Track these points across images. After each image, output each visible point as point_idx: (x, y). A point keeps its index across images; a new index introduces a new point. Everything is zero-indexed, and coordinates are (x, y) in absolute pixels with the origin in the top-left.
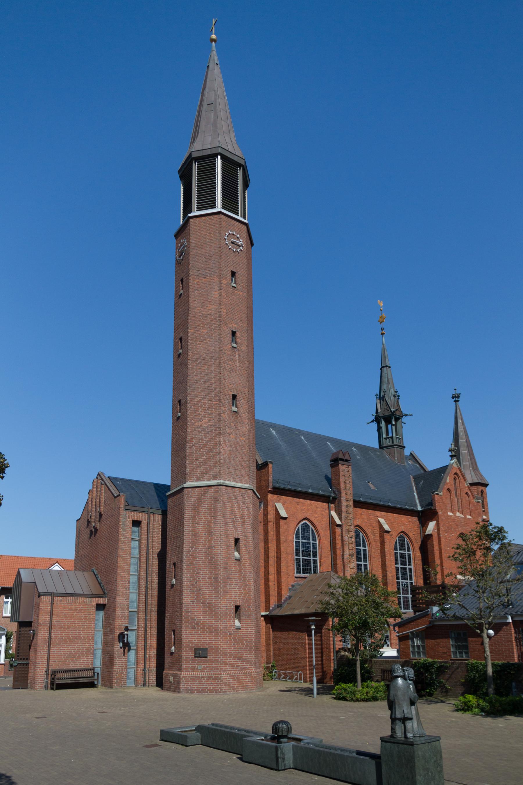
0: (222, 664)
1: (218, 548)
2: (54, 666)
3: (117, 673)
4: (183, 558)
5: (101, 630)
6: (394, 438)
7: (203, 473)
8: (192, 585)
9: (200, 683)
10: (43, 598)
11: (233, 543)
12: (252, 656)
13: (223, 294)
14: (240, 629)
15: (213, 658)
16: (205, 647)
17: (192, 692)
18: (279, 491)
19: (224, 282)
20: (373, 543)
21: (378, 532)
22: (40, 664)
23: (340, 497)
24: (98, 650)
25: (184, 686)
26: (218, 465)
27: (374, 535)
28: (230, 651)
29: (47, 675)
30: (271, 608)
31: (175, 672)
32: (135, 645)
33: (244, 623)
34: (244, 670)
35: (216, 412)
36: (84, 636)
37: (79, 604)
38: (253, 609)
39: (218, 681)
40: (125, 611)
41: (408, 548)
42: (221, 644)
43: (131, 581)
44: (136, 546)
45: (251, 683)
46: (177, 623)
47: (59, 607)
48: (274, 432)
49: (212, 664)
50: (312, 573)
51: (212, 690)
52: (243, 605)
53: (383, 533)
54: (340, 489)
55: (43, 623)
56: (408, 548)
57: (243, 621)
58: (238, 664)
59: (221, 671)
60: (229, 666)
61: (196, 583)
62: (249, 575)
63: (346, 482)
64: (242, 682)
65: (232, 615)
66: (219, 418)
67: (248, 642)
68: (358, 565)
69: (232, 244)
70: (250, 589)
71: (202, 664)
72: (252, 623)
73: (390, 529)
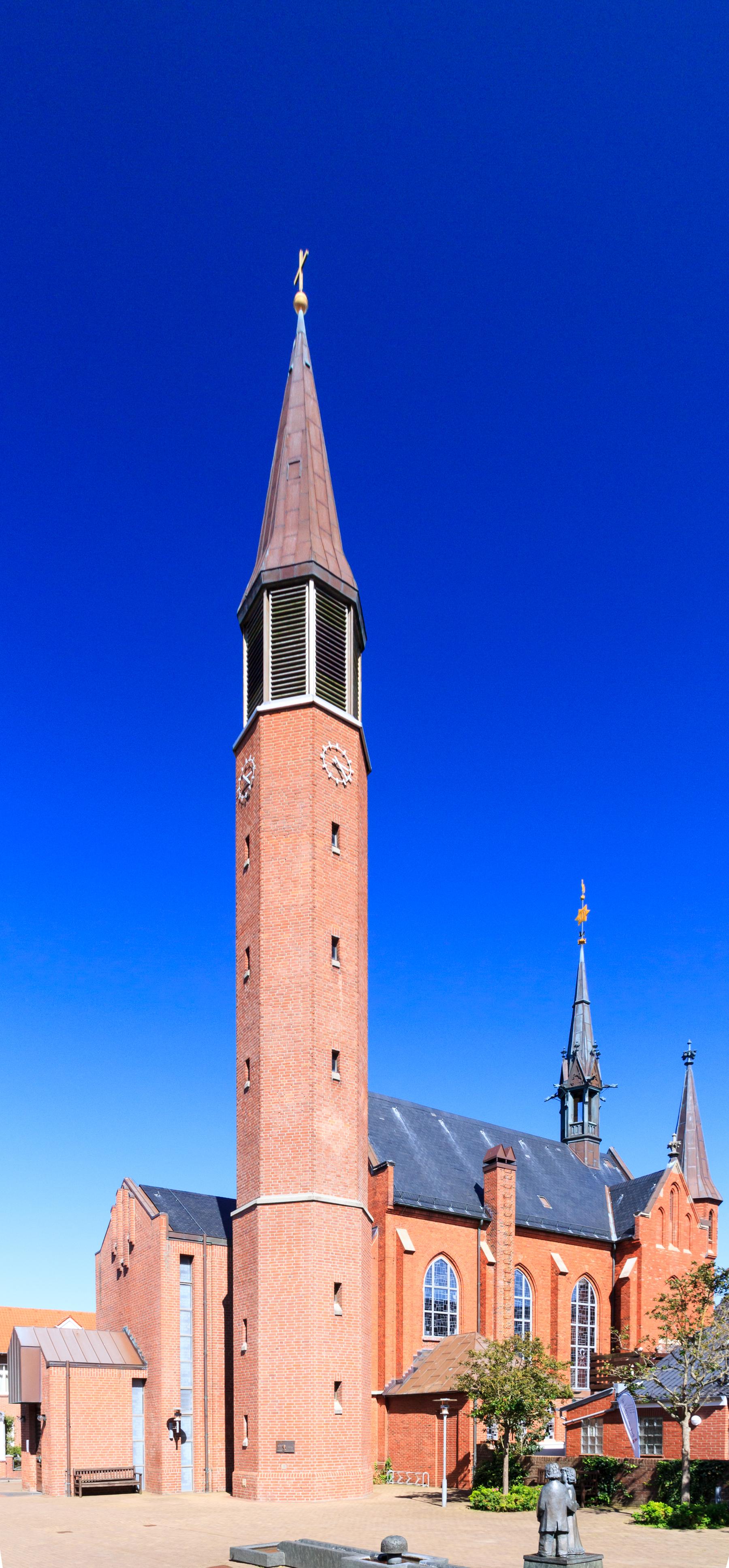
0: (315, 1462)
2: (76, 1466)
3: (167, 1474)
8: (272, 1352)
10: (54, 1370)
16: (292, 1439)
33: (347, 1407)
38: (360, 1387)
40: (175, 1388)
46: (250, 1406)
53: (557, 1275)
56: (592, 1298)
57: (346, 1404)
58: (338, 1462)
59: (313, 1472)
60: (325, 1465)
66: (310, 1091)
68: (516, 1323)
71: (288, 1463)
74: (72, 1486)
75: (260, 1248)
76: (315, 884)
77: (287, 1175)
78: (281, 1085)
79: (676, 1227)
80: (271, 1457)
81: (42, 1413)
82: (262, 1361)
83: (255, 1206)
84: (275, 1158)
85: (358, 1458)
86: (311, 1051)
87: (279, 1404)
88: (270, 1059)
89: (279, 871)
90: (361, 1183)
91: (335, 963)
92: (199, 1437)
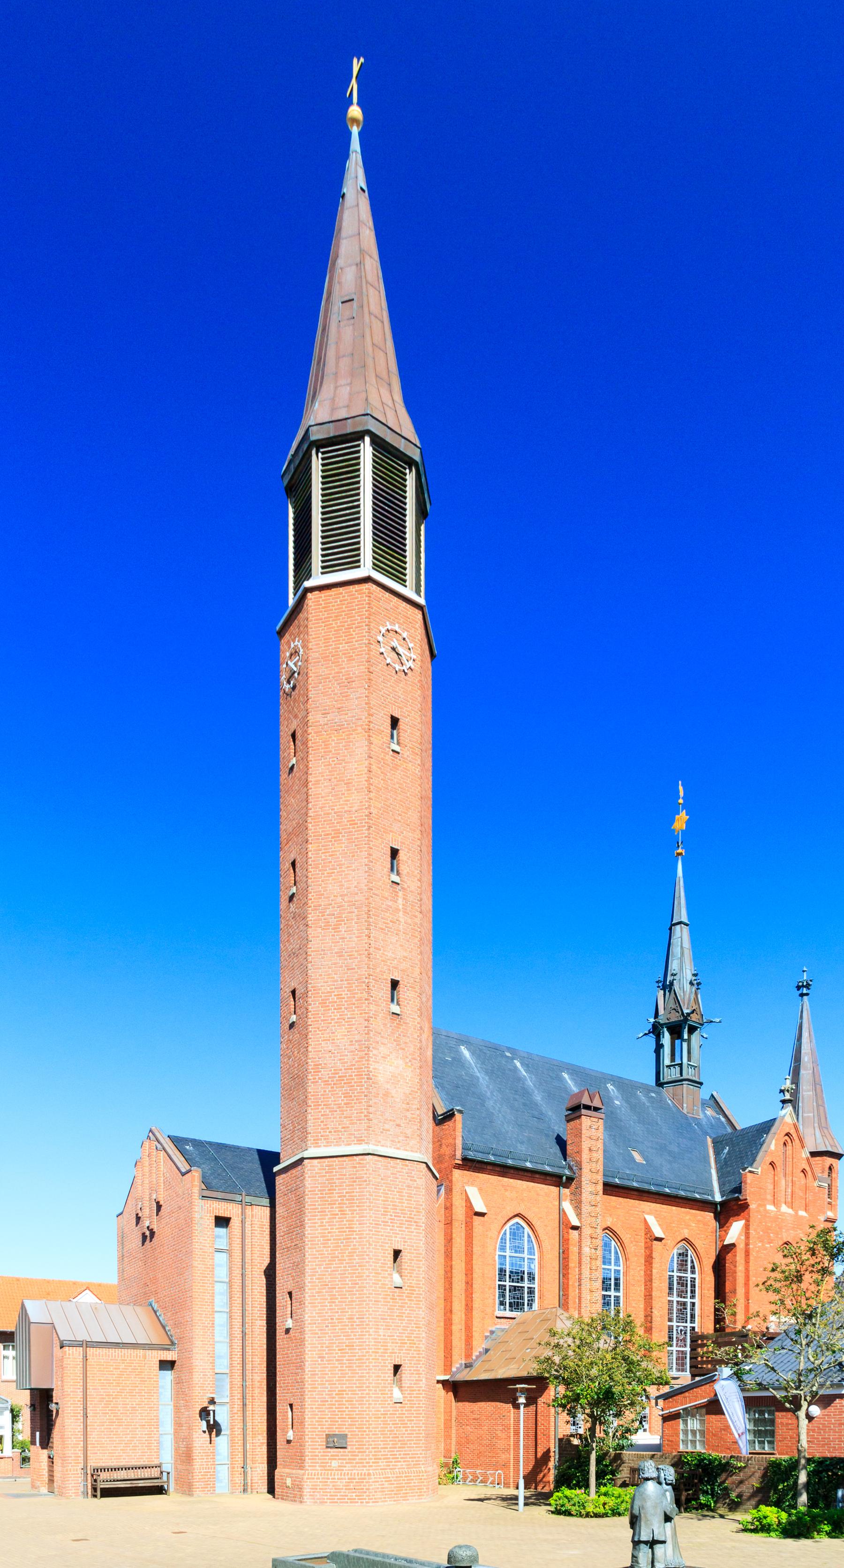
7: (338, 1131)
10: (69, 1350)
13: (374, 767)
30: (454, 1369)
38: (423, 1371)
43: (216, 1322)
53: (651, 1240)
56: (693, 1267)
59: (369, 1470)
62: (417, 1314)
64: (404, 1487)
66: (365, 1027)
68: (604, 1297)
71: (339, 1459)
75: (307, 1209)
76: (371, 787)
77: (339, 1124)
79: (790, 1184)
80: (320, 1452)
83: (302, 1160)
85: (421, 1454)
90: (424, 1133)
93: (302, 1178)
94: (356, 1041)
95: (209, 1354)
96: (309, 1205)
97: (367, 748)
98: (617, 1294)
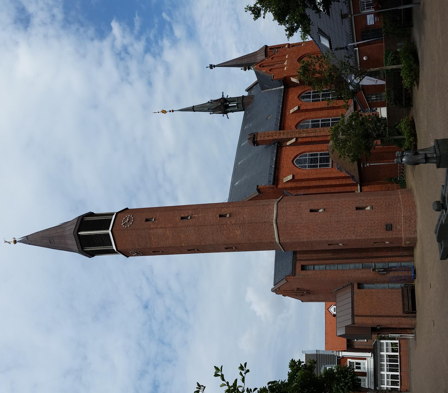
0: (397, 216)
1: (317, 221)
2: (400, 312)
3: (405, 274)
4: (325, 240)
5: (375, 285)
6: (238, 102)
9: (410, 227)
10: (356, 321)
11: (313, 213)
12: (390, 197)
13: (160, 226)
14: (372, 207)
15: (392, 221)
17: (416, 231)
18: (276, 179)
19: (152, 226)
20: (307, 116)
21: (299, 113)
22: (399, 322)
23: (277, 139)
24: (389, 286)
25: (412, 235)
26: (264, 223)
27: (301, 116)
28: (387, 212)
29: (406, 317)
30: (355, 182)
31: (403, 241)
32: (385, 263)
33: (368, 204)
34: (400, 202)
35: (231, 226)
36: (380, 296)
37: (358, 300)
38: (358, 198)
39: (408, 218)
40: (362, 271)
41: (308, 93)
42: (383, 217)
43: (341, 269)
44: (318, 267)
45: (409, 197)
46: (369, 241)
47: (361, 312)
48: (237, 183)
49: (397, 221)
50: (329, 156)
51: (414, 221)
52: (355, 205)
53: (299, 110)
54: (273, 139)
55: (372, 321)
56: (308, 93)
57: (367, 204)
58: (396, 207)
59: (401, 216)
60: (398, 212)
61: (341, 232)
62: (335, 202)
63: (268, 135)
64: (409, 203)
65: (363, 212)
66: (235, 225)
67: (381, 201)
68: (322, 126)
69: (130, 222)
70: (344, 201)
71: (397, 226)
72: (368, 198)
73: (297, 106)
74: (411, 315)
75: (297, 241)
76: (165, 227)
77: (267, 232)
78: (233, 235)
81: (376, 327)
82: (347, 238)
83: (280, 243)
84: (261, 236)
85: (394, 197)
86: (220, 225)
87: (368, 231)
88: (225, 241)
89: (162, 241)
90: (268, 203)
91: (189, 218)
92: (386, 260)
93: (286, 243)
94: (239, 228)
95: (354, 271)
96: (296, 241)
97: (155, 229)
98: (320, 121)
